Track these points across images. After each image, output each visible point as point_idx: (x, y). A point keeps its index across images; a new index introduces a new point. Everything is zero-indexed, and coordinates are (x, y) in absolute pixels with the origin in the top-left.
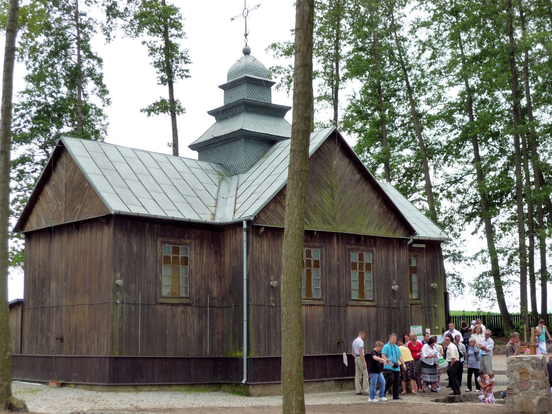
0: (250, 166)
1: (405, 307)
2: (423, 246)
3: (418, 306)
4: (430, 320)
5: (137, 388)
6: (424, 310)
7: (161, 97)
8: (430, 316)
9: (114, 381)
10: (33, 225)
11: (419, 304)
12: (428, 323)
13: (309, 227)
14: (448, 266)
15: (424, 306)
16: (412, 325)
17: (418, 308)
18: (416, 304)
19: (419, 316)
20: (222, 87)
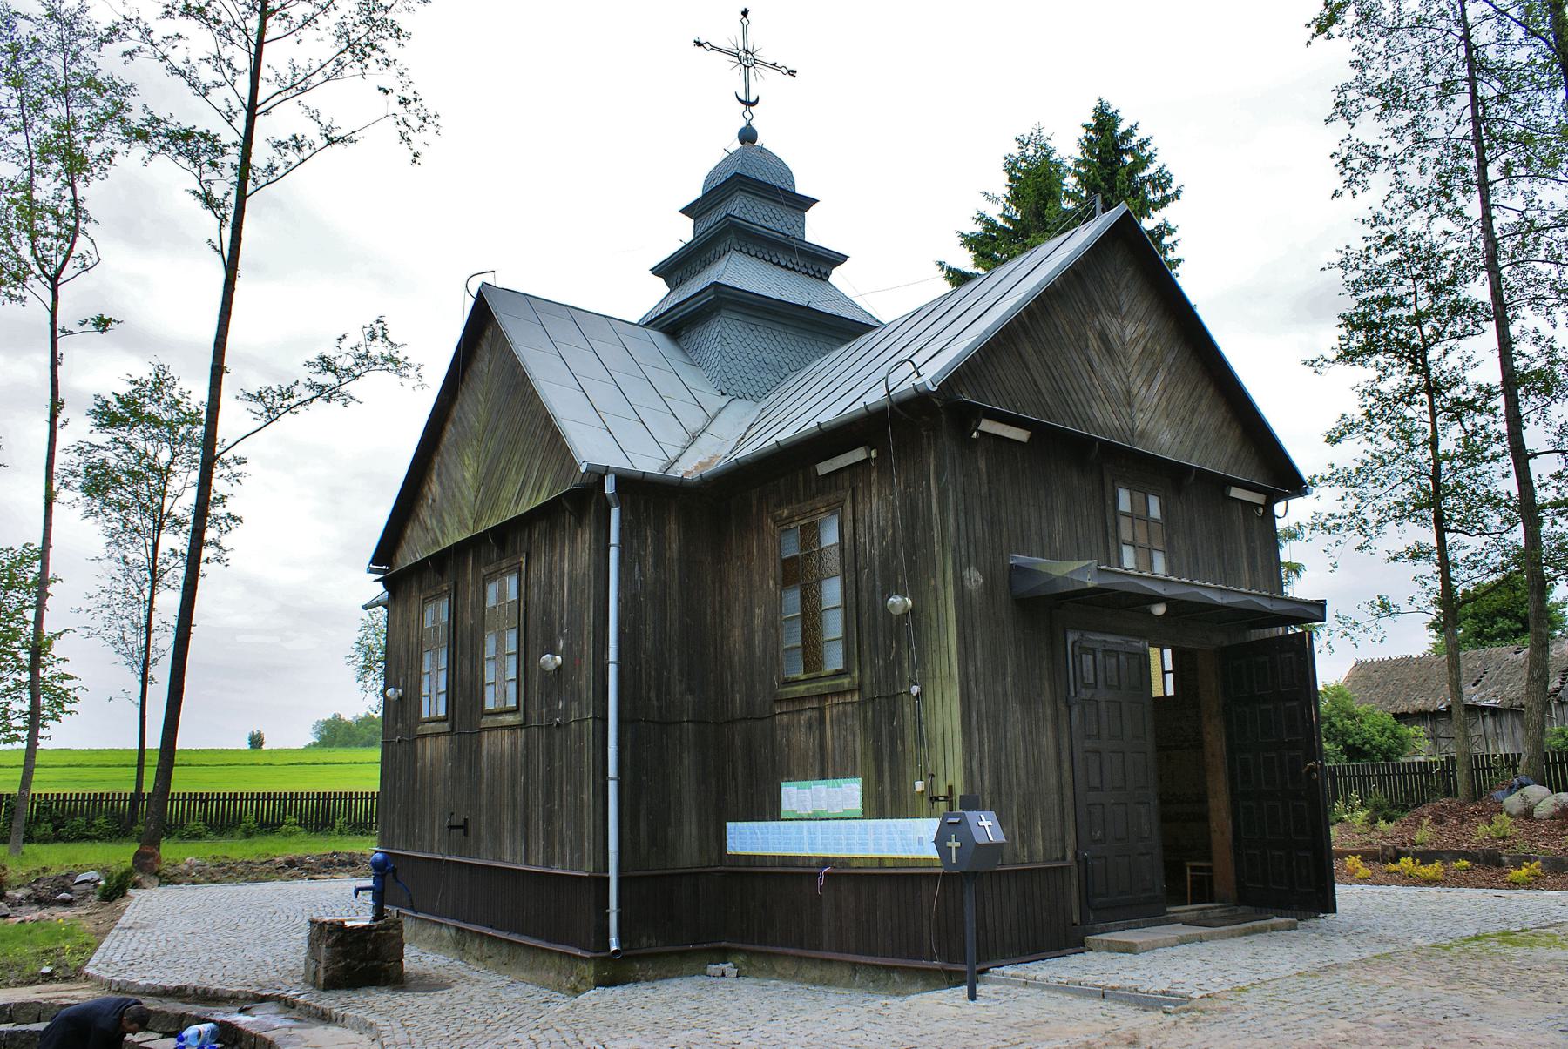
0: (790, 266)
1: (581, 721)
2: (1021, 435)
3: (848, 698)
4: (893, 752)
5: (541, 959)
6: (870, 714)
7: (1118, 111)
8: (896, 736)
9: (1242, 900)
10: (409, 556)
11: (851, 691)
12: (886, 765)
13: (1091, 429)
14: (188, 544)
15: (868, 695)
16: (790, 777)
17: (849, 708)
18: (833, 694)
19: (850, 738)
20: (687, 211)
